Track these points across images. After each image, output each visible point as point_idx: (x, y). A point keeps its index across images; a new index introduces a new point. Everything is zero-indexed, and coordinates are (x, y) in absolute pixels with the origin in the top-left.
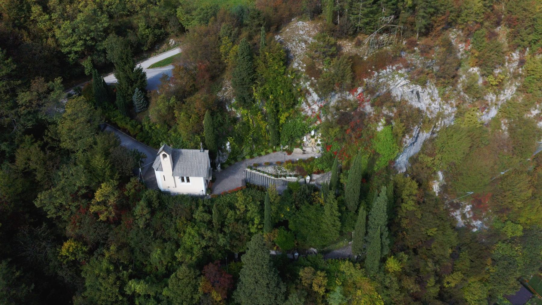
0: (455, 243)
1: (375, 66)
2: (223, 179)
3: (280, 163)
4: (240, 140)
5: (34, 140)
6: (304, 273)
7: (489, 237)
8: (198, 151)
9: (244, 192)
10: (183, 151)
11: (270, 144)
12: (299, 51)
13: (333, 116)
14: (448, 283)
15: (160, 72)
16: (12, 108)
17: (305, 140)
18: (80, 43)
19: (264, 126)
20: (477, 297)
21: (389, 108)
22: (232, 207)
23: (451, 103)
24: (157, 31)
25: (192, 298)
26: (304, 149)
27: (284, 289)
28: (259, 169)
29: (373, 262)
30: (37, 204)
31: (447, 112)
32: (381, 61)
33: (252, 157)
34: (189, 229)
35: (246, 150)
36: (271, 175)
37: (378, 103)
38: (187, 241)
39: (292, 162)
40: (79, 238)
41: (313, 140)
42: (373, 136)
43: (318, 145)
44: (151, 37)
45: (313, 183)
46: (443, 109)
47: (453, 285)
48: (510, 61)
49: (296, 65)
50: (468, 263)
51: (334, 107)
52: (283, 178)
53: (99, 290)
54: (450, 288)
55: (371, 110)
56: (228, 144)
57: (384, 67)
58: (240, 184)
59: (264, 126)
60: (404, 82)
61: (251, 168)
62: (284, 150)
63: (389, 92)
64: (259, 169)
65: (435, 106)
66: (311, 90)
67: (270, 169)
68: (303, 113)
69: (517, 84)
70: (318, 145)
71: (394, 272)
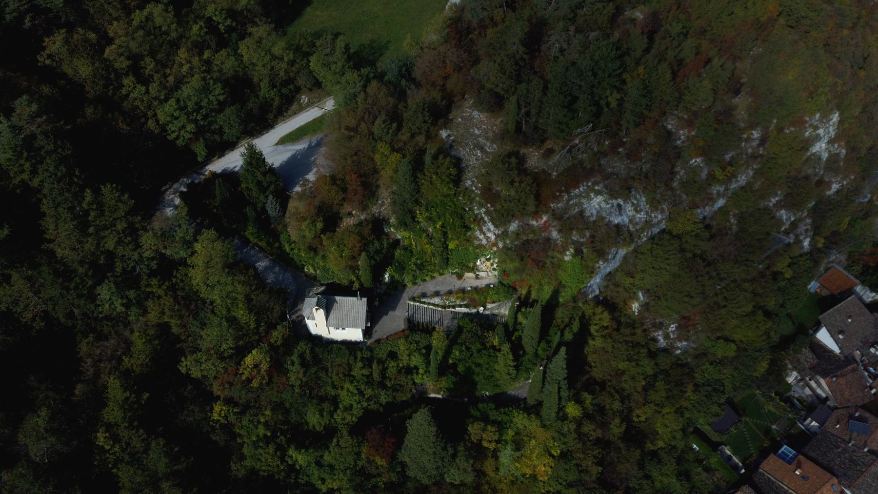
0: (650, 371)
2: (381, 317)
3: (450, 293)
4: (401, 268)
6: (474, 430)
7: (696, 357)
8: (355, 299)
9: (407, 337)
10: (337, 298)
11: (437, 268)
12: (473, 161)
13: (512, 242)
14: (638, 416)
15: (293, 152)
16: (134, 250)
17: (478, 263)
19: (429, 249)
20: (669, 430)
22: (393, 355)
23: (662, 209)
24: (284, 91)
25: (356, 465)
27: (451, 451)
29: (549, 411)
30: (183, 370)
31: (655, 220)
32: (575, 176)
34: (347, 385)
36: (438, 306)
37: (566, 228)
38: (345, 398)
39: (463, 291)
40: (229, 401)
41: (488, 263)
42: (558, 265)
43: (494, 269)
44: (277, 99)
45: (487, 312)
46: (651, 217)
47: (643, 419)
48: (748, 140)
49: (469, 183)
50: (664, 394)
51: (513, 232)
52: (452, 309)
53: (259, 460)
54: (640, 422)
55: (558, 237)
58: (402, 325)
59: (429, 249)
61: (413, 299)
63: (581, 213)
65: (642, 216)
66: (486, 219)
67: (437, 300)
68: (476, 242)
69: (755, 166)
70: (494, 269)
71: (574, 418)
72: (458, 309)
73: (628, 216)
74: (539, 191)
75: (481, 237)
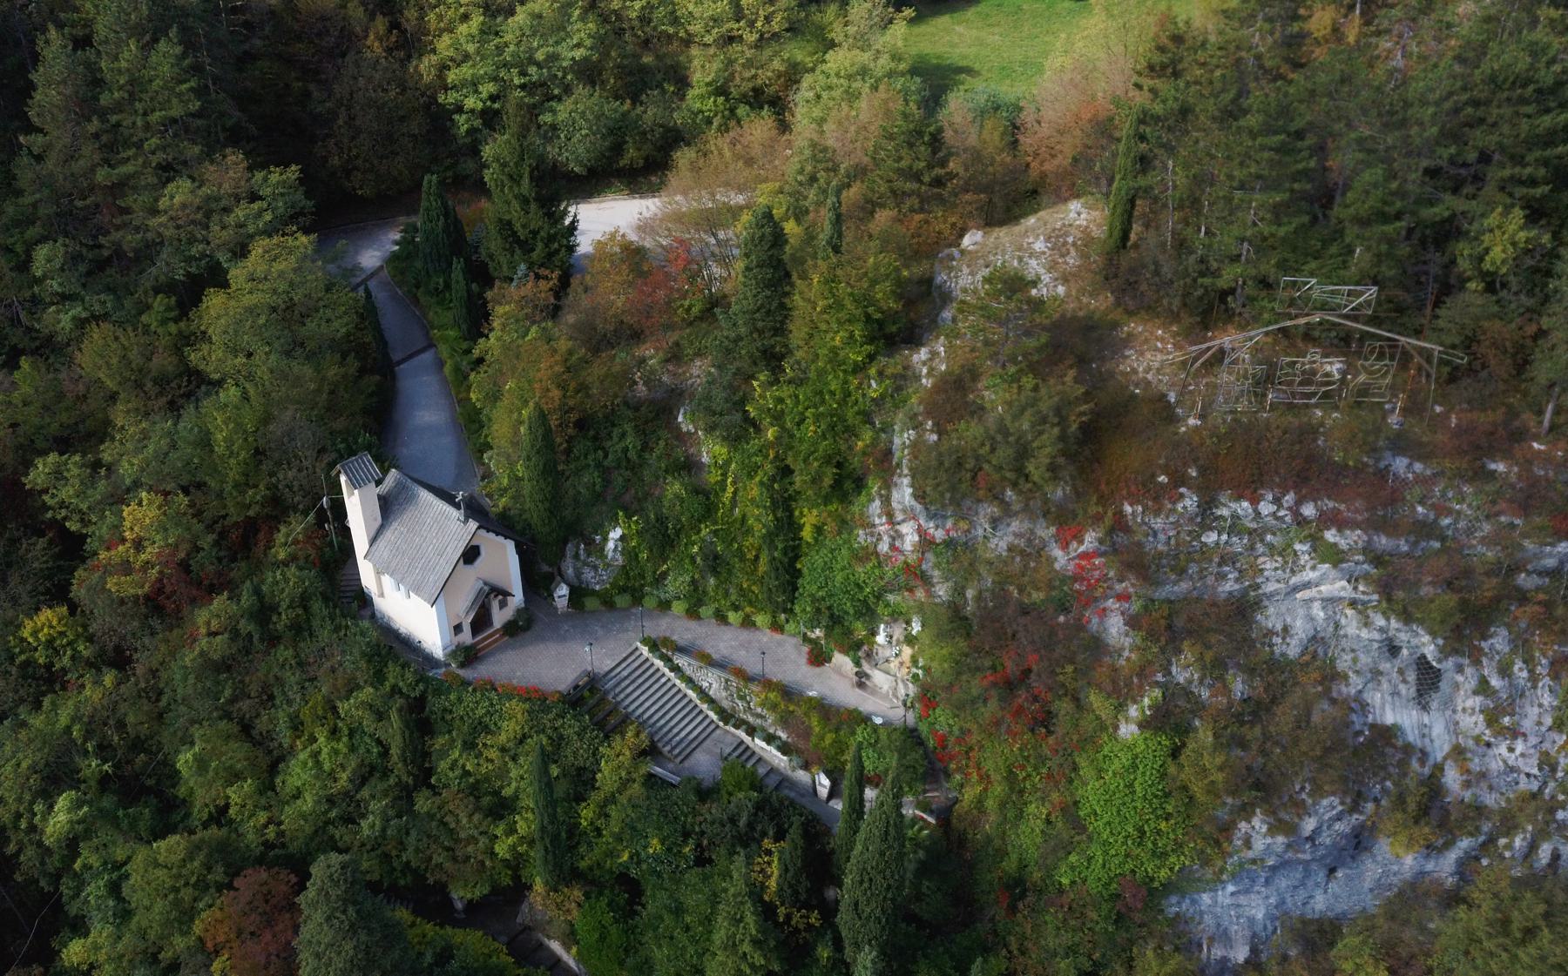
1: (1203, 471)
2: (543, 639)
4: (663, 539)
5: (173, 314)
10: (425, 496)
17: (881, 639)
18: (488, 88)
21: (1215, 669)
26: (866, 667)
28: (681, 661)
33: (693, 614)
35: (676, 583)
36: (711, 701)
52: (741, 734)
56: (616, 534)
57: (1249, 489)
60: (1338, 587)
61: (654, 646)
62: (806, 639)
63: (1245, 608)
64: (681, 661)
67: (712, 681)
72: (759, 744)
73: (1454, 728)
74: (1100, 442)
75: (880, 522)
